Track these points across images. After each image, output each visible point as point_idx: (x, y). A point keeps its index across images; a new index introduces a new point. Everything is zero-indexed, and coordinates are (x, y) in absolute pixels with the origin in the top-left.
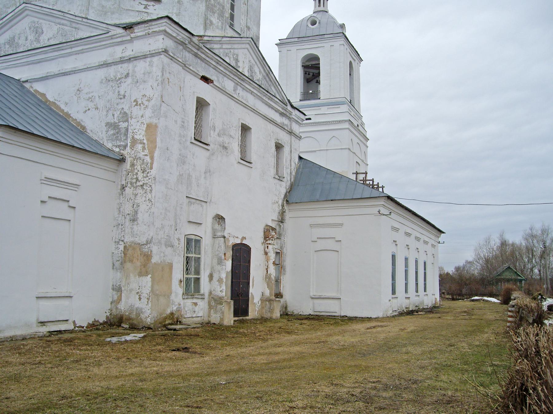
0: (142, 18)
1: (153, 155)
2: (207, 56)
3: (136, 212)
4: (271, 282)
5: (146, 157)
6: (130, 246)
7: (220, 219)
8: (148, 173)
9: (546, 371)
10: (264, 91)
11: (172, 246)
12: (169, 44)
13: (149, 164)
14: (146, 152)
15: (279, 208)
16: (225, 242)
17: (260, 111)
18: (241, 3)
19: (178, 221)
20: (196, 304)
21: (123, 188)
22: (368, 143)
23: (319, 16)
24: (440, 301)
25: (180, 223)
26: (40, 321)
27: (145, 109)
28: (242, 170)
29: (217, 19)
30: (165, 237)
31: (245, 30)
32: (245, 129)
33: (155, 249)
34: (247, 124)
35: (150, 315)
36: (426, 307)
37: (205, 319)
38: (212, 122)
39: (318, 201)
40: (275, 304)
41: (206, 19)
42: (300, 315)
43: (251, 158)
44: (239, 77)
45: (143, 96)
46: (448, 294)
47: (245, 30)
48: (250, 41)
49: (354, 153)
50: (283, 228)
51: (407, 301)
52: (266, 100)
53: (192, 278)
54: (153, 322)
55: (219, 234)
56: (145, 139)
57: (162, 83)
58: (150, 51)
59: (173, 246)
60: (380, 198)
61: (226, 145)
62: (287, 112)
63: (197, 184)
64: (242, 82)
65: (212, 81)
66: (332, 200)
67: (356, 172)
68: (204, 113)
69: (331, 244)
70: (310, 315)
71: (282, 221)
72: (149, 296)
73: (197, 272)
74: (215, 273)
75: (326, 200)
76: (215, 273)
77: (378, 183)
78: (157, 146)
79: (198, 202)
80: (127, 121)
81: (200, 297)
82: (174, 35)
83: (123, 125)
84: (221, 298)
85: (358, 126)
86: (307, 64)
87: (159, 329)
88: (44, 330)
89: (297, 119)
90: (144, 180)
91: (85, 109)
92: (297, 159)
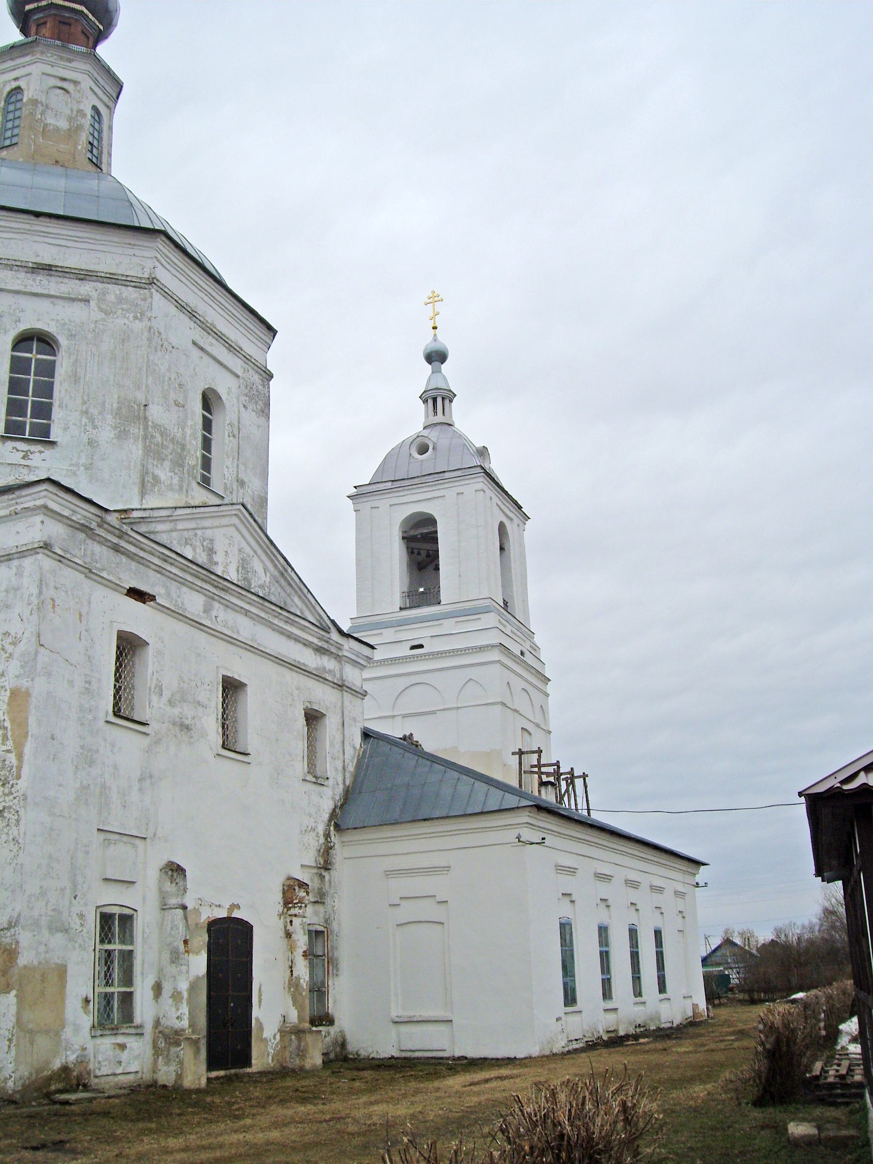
0: (17, 476)
1: (23, 751)
2: (141, 549)
4: (301, 994)
5: (9, 755)
7: (175, 870)
8: (12, 786)
10: (274, 607)
12: (56, 531)
13: (14, 769)
14: (10, 744)
15: (318, 841)
17: (265, 647)
18: (224, 434)
19: (80, 879)
20: (122, 1047)
22: (550, 688)
23: (433, 435)
24: (707, 1008)
25: (84, 882)
27: (8, 661)
29: (170, 472)
30: (50, 913)
31: (235, 487)
33: (25, 938)
34: (236, 677)
35: (13, 1075)
36: (669, 1025)
37: (144, 1076)
38: (155, 678)
39: (396, 823)
40: (309, 1038)
41: (144, 473)
42: (373, 1058)
43: (247, 745)
44: (216, 584)
45: (5, 634)
46: (742, 991)
47: (235, 487)
48: (239, 510)
49: (516, 711)
50: (330, 882)
51: (611, 1017)
52: (280, 625)
53: (113, 993)
54: (20, 1088)
55: (173, 901)
56: (7, 719)
58: (17, 547)
59: (67, 931)
60: (521, 810)
61: (187, 722)
62: (332, 645)
63: (121, 803)
64: (222, 594)
65: (152, 598)
66: (425, 820)
67: (520, 749)
68: (137, 661)
69: (427, 910)
70: (393, 1057)
71: (326, 865)
72: (13, 1035)
73: (128, 978)
74: (165, 980)
75: (414, 821)
76: (165, 980)
77: (572, 769)
78: (30, 734)
79: (125, 839)
81: (133, 1031)
82: (66, 513)
84: (178, 1032)
85: (522, 653)
86: (413, 533)
87: (34, 1104)
89: (354, 657)
90: (4, 801)
92: (358, 739)
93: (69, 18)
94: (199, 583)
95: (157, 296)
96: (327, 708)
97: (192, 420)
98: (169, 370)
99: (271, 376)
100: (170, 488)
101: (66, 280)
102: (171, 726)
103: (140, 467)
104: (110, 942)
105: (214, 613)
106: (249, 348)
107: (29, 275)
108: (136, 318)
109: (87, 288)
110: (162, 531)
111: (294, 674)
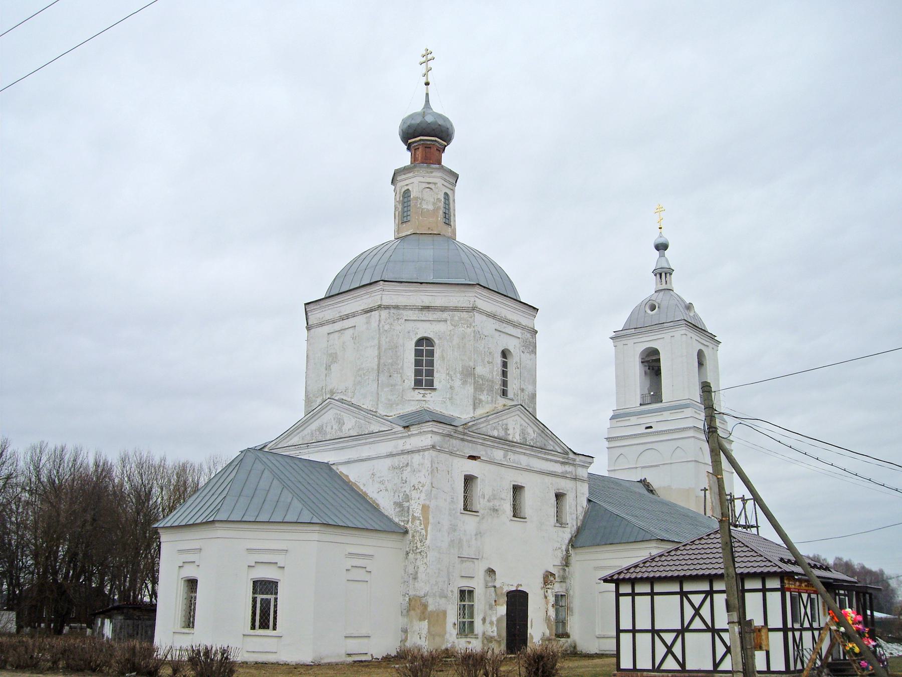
3: (417, 573)
6: (413, 598)
7: (491, 572)
11: (446, 597)
12: (437, 439)
14: (422, 526)
16: (495, 591)
19: (451, 577)
21: (407, 553)
26: (347, 653)
28: (517, 525)
30: (440, 591)
31: (519, 393)
32: (517, 489)
33: (430, 601)
41: (475, 399)
47: (519, 393)
52: (542, 456)
55: (490, 584)
57: (431, 473)
64: (512, 448)
67: (705, 488)
73: (472, 615)
79: (470, 560)
80: (409, 501)
83: (406, 504)
88: (350, 659)
89: (582, 464)
91: (378, 490)
93: (430, 144)
94: (501, 446)
95: (476, 314)
96: (568, 491)
97: (496, 367)
98: (484, 348)
99: (536, 332)
100: (487, 403)
101: (436, 312)
102: (489, 511)
103: (472, 397)
104: (464, 601)
105: (508, 457)
106: (524, 321)
107: (420, 312)
108: (468, 327)
109: (445, 315)
110: (484, 428)
111: (550, 477)
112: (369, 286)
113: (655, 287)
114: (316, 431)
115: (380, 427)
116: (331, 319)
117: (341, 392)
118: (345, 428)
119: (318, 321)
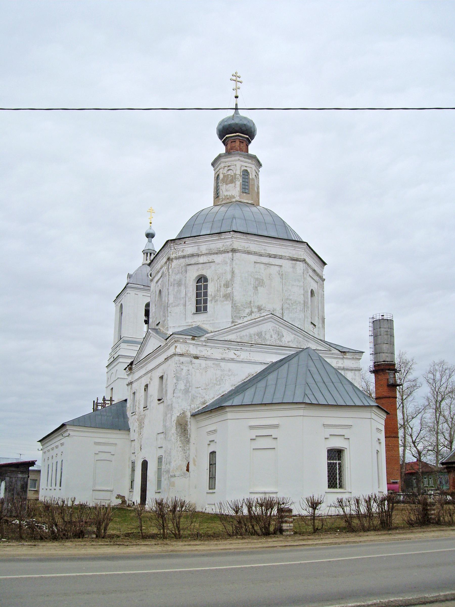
9: (102, 524)
112: (288, 241)
113: (142, 261)
114: (254, 335)
115: (317, 346)
116: (259, 252)
117: (269, 311)
118: (273, 339)
119: (242, 248)
